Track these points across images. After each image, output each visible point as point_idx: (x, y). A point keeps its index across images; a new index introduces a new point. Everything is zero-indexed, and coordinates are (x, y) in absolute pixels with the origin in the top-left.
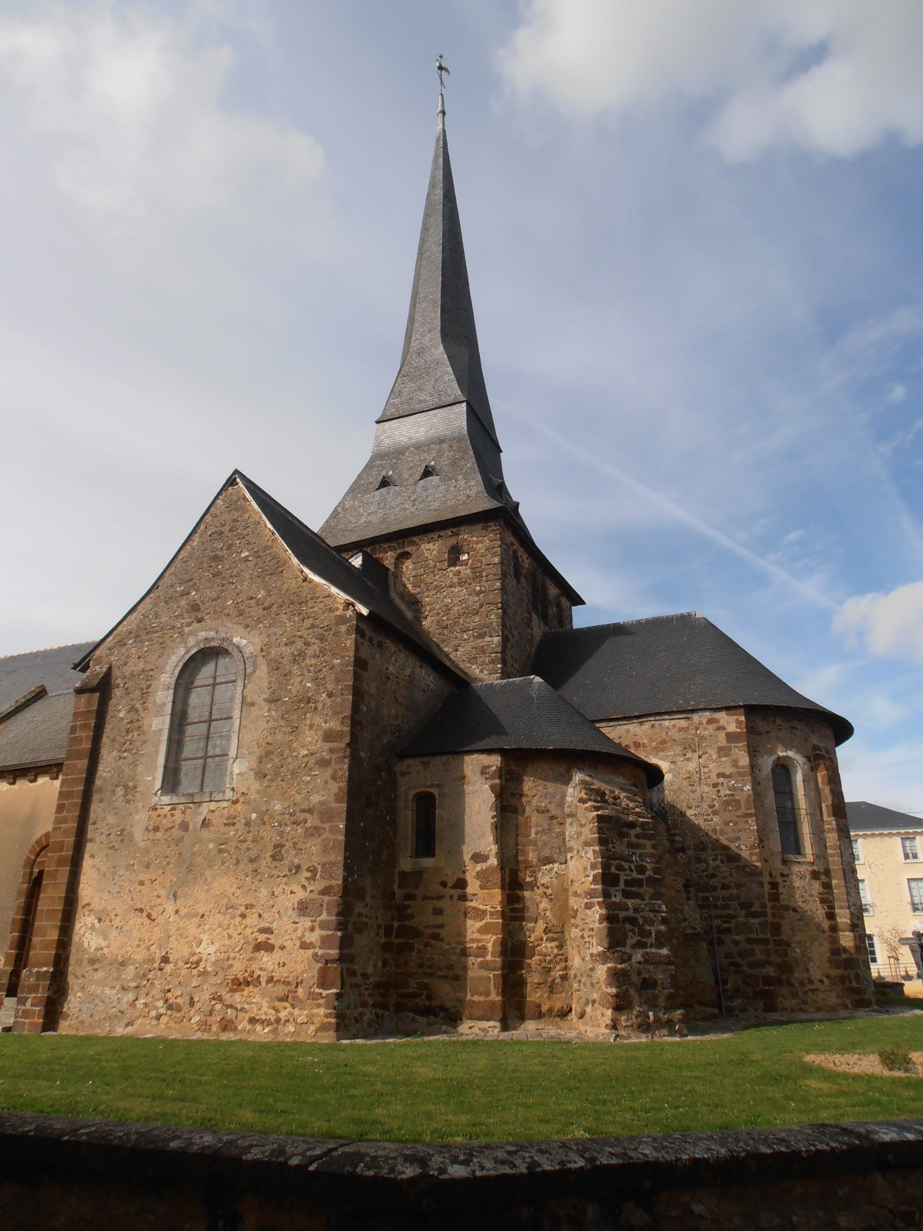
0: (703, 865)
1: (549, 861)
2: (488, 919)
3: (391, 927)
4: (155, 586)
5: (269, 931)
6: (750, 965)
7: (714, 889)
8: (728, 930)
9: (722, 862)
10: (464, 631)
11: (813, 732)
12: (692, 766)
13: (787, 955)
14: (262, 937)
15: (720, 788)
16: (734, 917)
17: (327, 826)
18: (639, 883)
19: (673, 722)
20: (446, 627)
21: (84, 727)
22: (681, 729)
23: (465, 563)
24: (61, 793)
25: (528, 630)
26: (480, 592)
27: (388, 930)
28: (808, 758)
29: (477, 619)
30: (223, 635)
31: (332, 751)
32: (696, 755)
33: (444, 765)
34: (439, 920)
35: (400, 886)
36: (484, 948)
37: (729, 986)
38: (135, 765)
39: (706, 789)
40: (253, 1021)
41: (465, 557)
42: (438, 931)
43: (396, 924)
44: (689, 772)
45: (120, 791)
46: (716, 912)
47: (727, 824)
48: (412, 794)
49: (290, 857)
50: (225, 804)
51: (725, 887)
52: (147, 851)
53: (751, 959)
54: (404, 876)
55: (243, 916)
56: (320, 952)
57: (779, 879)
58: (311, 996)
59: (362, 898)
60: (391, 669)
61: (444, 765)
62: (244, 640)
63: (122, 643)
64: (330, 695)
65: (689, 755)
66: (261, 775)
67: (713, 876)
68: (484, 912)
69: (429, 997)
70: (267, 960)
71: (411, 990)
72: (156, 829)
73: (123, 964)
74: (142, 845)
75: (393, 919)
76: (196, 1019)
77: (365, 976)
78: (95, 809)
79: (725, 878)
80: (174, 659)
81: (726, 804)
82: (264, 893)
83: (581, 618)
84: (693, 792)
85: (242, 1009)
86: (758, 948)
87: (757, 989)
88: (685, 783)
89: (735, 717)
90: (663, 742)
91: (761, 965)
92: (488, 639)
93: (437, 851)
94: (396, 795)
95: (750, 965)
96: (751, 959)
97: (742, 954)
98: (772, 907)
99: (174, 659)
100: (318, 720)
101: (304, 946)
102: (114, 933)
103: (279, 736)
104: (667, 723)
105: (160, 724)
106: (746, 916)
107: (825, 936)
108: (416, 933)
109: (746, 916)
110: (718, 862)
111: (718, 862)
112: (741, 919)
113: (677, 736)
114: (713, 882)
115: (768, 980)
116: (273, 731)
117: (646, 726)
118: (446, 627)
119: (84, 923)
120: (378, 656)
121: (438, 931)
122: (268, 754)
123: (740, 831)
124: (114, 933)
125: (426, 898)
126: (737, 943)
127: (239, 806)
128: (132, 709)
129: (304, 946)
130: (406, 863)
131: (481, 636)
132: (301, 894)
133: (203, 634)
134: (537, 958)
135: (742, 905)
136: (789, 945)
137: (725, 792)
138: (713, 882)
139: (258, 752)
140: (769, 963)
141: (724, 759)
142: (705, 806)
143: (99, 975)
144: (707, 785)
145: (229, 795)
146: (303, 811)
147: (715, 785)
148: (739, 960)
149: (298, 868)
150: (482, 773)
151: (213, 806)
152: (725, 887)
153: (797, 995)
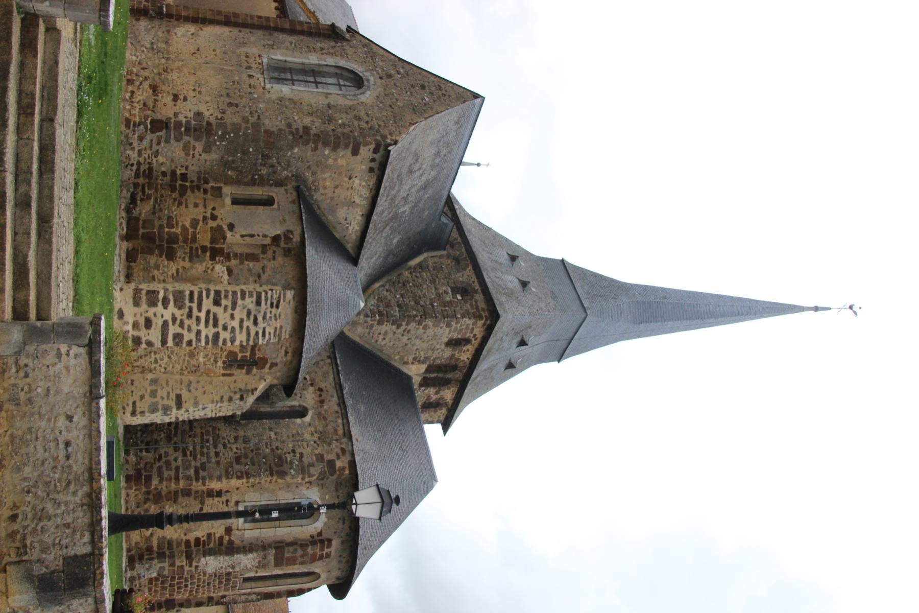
0: (232, 441)
1: (230, 272)
2: (191, 230)
3: (186, 180)
4: (399, 59)
5: (185, 99)
6: (160, 468)
7: (215, 446)
8: (185, 455)
9: (236, 453)
10: (402, 296)
11: (342, 543)
12: (307, 436)
13: (168, 500)
14: (181, 97)
15: (292, 454)
16: (195, 459)
17: (249, 125)
18: (215, 325)
19: (341, 426)
20: (404, 285)
21: (311, 28)
22: (336, 431)
23: (454, 297)
24: (268, 18)
25: (411, 359)
26: (433, 306)
27: (184, 177)
28: (320, 534)
29: (412, 303)
30: (372, 87)
31: (297, 129)
32: (316, 439)
33: (293, 212)
34: (191, 206)
35: (212, 187)
36: (173, 227)
37: (144, 453)
38: (287, 49)
39: (290, 445)
40: (133, 92)
41: (459, 297)
42: (184, 205)
43: (188, 184)
44: (303, 434)
45: (270, 43)
46: (198, 448)
47: (264, 457)
48: (274, 195)
49: (230, 110)
50: (262, 84)
51: (217, 454)
52: (234, 53)
53: (164, 468)
54: (220, 189)
55: (194, 90)
56: (172, 121)
57: (224, 498)
58: (146, 117)
59: (205, 151)
60: (357, 181)
61: (293, 212)
62: (367, 97)
63: (364, 46)
64: (333, 130)
65: (316, 435)
66: (281, 99)
67: (225, 446)
68: (196, 228)
69: (142, 200)
70: (168, 99)
71: (147, 190)
72: (247, 57)
73: (167, 43)
74: (238, 51)
75: (192, 182)
76: (135, 70)
77: (157, 154)
78: (259, 33)
79: (224, 454)
80: (356, 66)
81: (280, 458)
82: (208, 99)
83: (432, 431)
84: (288, 436)
85: (139, 88)
86: (172, 473)
87: (143, 471)
88: (294, 432)
89: (347, 466)
90: (325, 418)
91: (160, 474)
92: (397, 309)
93: (235, 206)
94: (271, 185)
95: (160, 468)
96: (164, 468)
97: (168, 463)
98: (203, 491)
99: (356, 66)
100: (317, 124)
101: (176, 115)
102: (185, 39)
103: (306, 108)
104: (340, 421)
105: (313, 59)
106: (196, 467)
107: (182, 535)
108: (182, 194)
109: (196, 467)
110: (235, 450)
111: (235, 450)
112: (193, 463)
113: (330, 428)
114: (220, 447)
115: (149, 479)
116: (310, 105)
117: (336, 408)
118: (404, 285)
119: (192, 28)
120: (364, 167)
121: (184, 205)
122: (295, 103)
123: (259, 466)
124: (185, 39)
125: (205, 200)
126: (176, 460)
127: (261, 90)
128: (322, 49)
129: (176, 115)
130: (227, 190)
131: (399, 306)
132: (207, 114)
133: (372, 79)
134: (166, 263)
135: (203, 465)
136: (175, 502)
137: (289, 457)
138: (220, 447)
139: (296, 98)
140: (161, 481)
141: (314, 458)
142: (278, 444)
143: (160, 34)
144: (294, 446)
145: (268, 86)
146: (259, 116)
147: (294, 451)
148: (164, 460)
149: (224, 113)
150: (288, 231)
151: (261, 79)
152: (217, 454)
153: (138, 507)
